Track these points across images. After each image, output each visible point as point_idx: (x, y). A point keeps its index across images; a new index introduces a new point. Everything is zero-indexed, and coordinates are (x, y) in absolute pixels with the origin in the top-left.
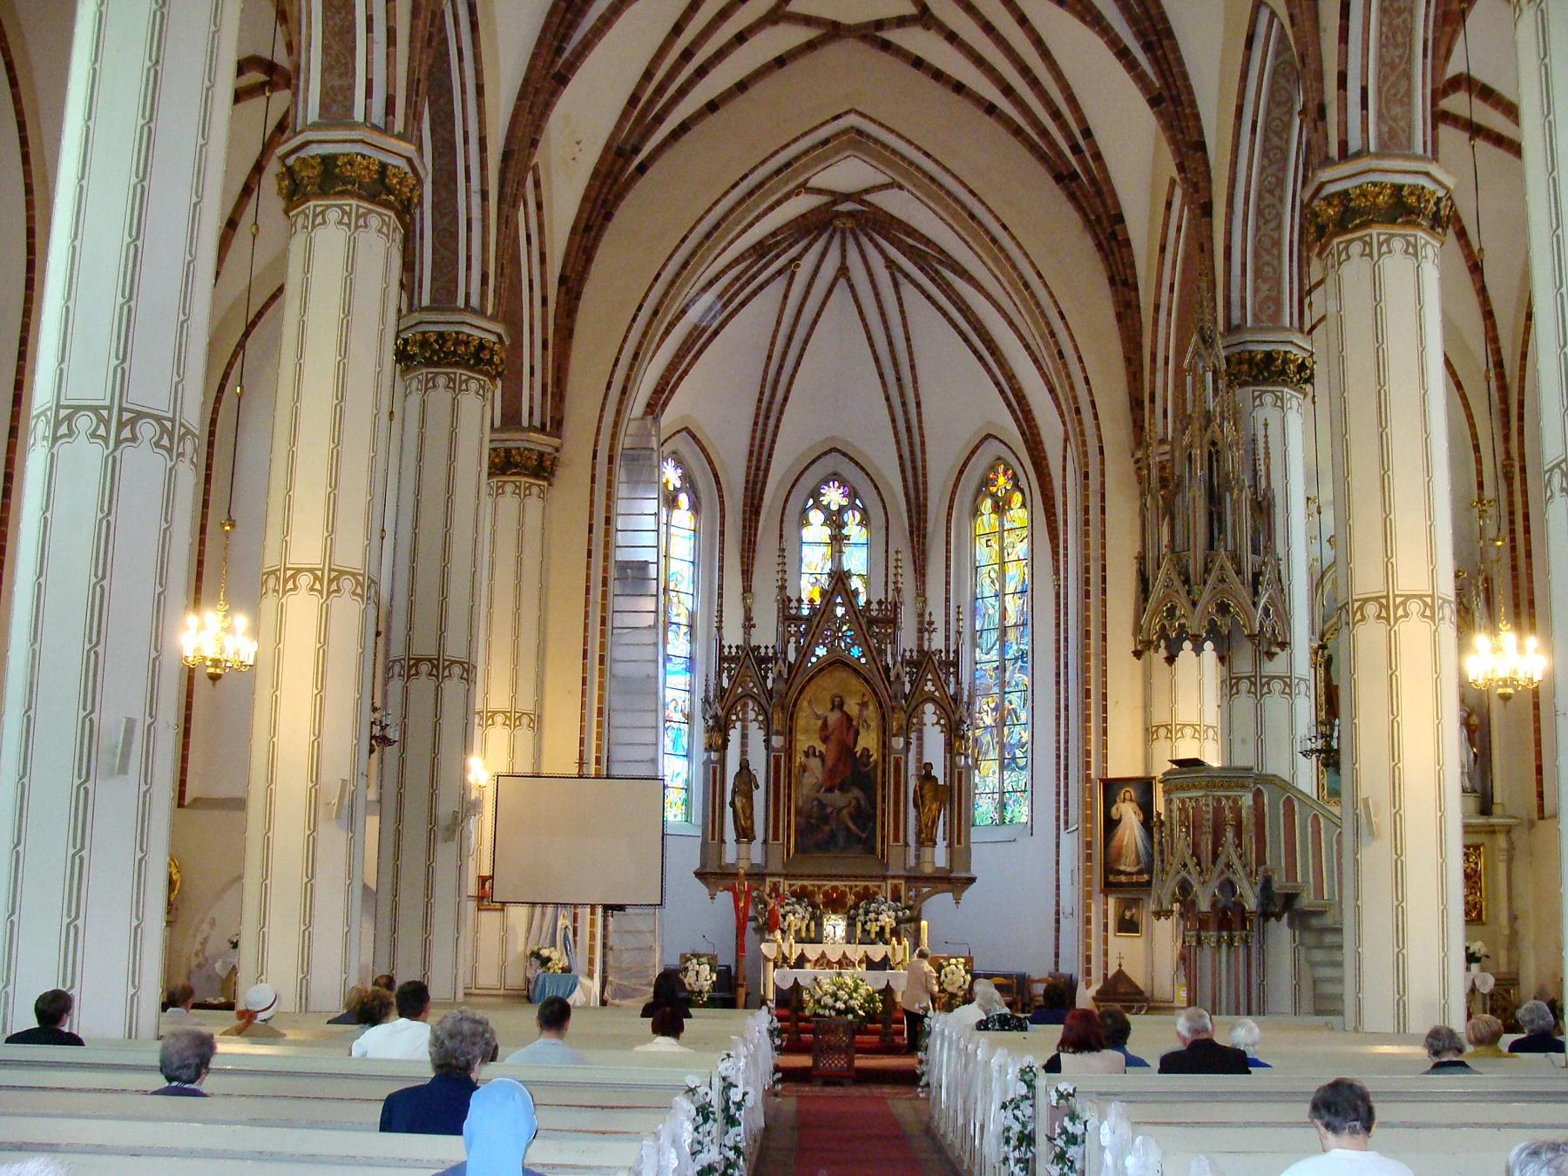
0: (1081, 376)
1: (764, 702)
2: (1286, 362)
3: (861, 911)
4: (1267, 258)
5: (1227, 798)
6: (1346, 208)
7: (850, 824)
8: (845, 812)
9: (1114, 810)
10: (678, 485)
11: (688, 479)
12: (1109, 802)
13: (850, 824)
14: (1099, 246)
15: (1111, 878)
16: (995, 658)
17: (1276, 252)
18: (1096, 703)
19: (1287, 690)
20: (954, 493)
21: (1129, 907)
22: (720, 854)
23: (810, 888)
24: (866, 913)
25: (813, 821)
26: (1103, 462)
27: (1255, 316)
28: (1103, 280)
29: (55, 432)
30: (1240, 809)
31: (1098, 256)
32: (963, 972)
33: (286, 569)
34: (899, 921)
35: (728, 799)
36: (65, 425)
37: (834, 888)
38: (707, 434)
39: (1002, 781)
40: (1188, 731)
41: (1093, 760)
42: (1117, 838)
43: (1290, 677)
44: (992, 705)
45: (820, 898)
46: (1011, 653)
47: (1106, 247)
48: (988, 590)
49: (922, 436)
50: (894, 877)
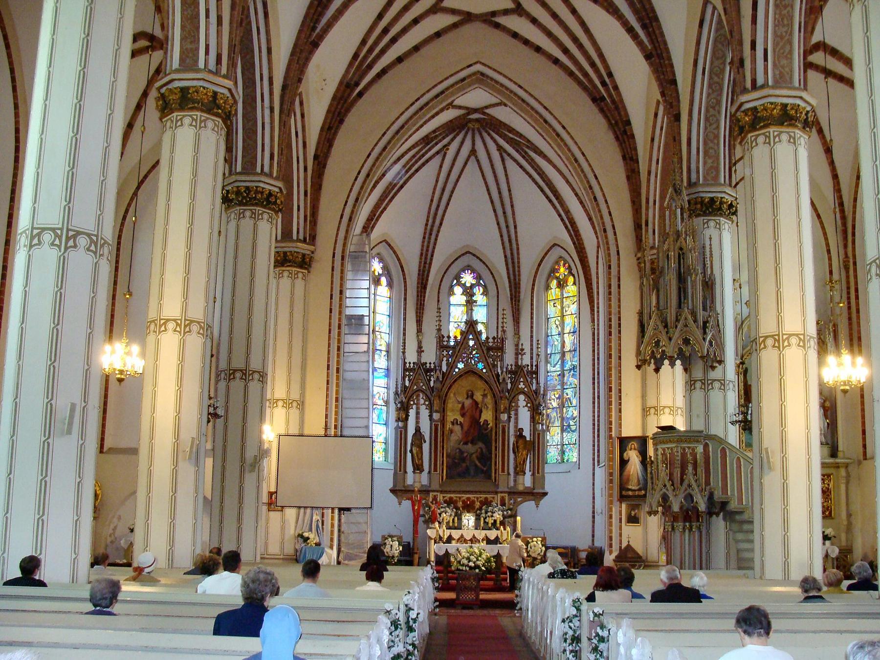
0: (607, 211)
1: (429, 394)
2: (721, 203)
3: (483, 511)
4: (711, 145)
5: (689, 448)
6: (756, 117)
7: (477, 462)
8: (474, 456)
9: (625, 454)
10: (381, 272)
11: (386, 269)
12: (622, 450)
13: (477, 462)
14: (617, 138)
15: (624, 493)
16: (558, 369)
17: (716, 142)
18: (615, 394)
19: (722, 387)
20: (535, 277)
21: (633, 509)
22: (404, 479)
23: (455, 498)
24: (486, 512)
25: (456, 461)
26: (619, 259)
27: (704, 177)
28: (619, 157)
29: (31, 242)
30: (696, 454)
31: (616, 144)
32: (541, 546)
33: (161, 319)
34: (504, 517)
35: (409, 448)
36: (37, 239)
37: (468, 499)
38: (397, 244)
39: (562, 438)
40: (667, 410)
41: (613, 426)
42: (627, 470)
43: (724, 380)
44: (557, 396)
45: (460, 504)
46: (567, 367)
47: (621, 139)
48: (555, 331)
49: (517, 245)
50: (501, 492)
